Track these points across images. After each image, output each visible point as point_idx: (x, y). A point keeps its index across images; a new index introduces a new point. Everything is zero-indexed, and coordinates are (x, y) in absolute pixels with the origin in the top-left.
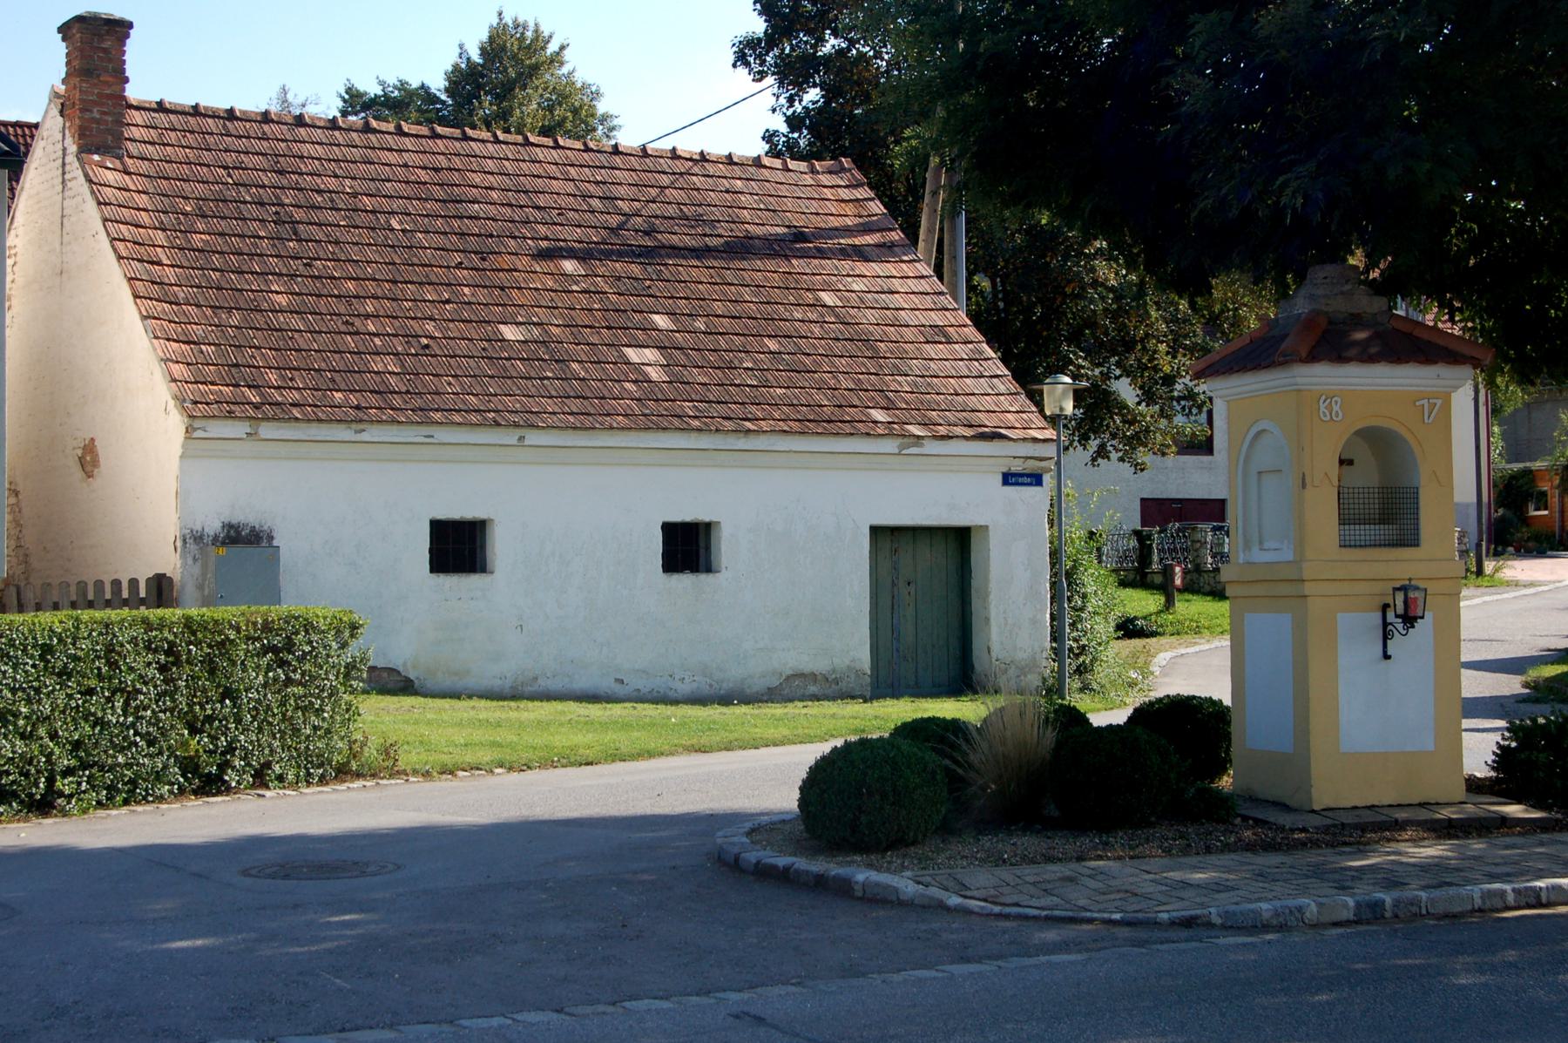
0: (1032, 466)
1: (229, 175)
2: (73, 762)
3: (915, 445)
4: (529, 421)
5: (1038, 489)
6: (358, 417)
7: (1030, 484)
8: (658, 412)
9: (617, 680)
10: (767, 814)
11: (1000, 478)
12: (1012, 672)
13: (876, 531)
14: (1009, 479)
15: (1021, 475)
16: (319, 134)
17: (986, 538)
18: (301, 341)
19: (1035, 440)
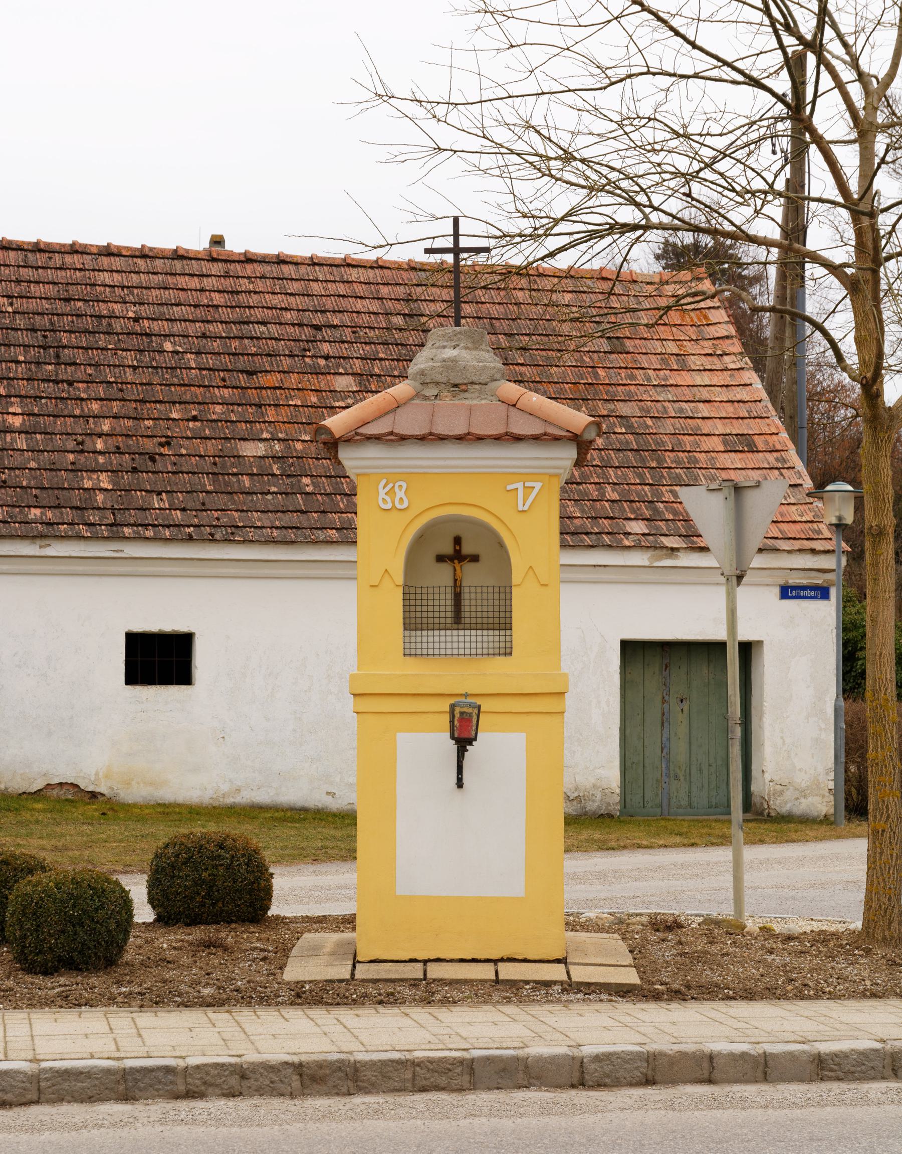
0: (819, 580)
1: (11, 304)
2: (33, 827)
3: (669, 557)
4: (232, 535)
5: (825, 602)
6: (47, 533)
7: (815, 598)
8: (119, 522)
9: (328, 793)
10: (47, 1003)
11: (777, 591)
12: (789, 794)
13: (629, 648)
14: (787, 592)
15: (804, 588)
16: (195, 266)
17: (761, 653)
18: (631, 475)
19: (813, 551)
